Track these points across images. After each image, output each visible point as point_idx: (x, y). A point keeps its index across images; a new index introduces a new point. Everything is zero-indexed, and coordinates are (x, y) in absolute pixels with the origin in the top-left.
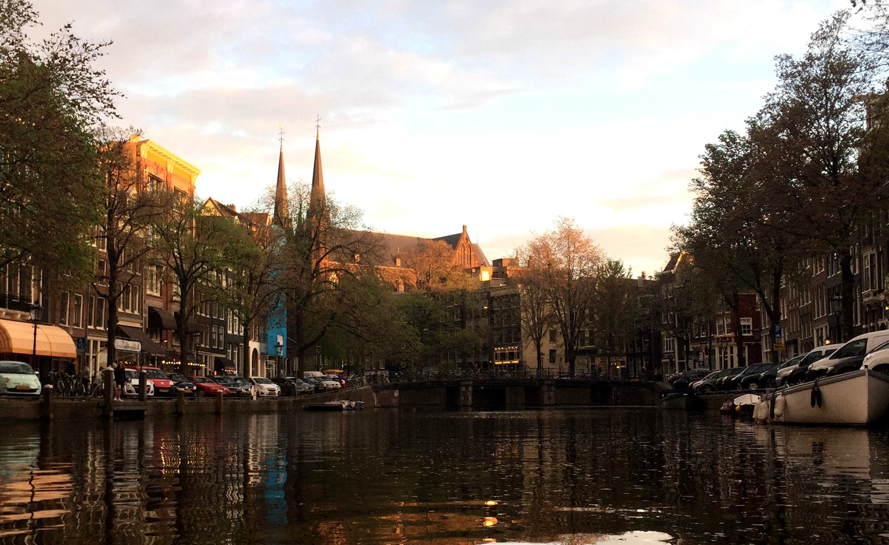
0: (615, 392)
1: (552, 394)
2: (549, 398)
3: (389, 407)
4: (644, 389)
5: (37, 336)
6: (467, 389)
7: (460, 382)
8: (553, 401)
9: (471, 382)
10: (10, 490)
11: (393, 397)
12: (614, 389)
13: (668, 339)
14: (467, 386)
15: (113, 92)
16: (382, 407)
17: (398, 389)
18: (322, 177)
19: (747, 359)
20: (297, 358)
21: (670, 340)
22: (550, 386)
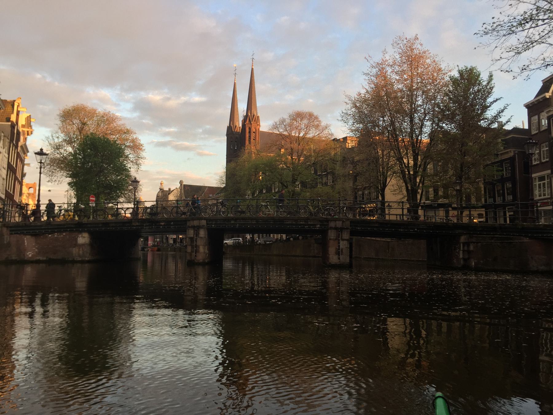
0: (464, 244)
1: (344, 245)
2: (338, 252)
3: (63, 262)
4: (526, 240)
5: (39, 172)
6: (197, 234)
7: (186, 221)
8: (345, 258)
9: (204, 222)
10: (14, 340)
11: (76, 245)
12: (463, 239)
13: (542, 182)
14: (197, 229)
15: (435, 145)
16: (50, 262)
17: (85, 232)
18: (255, 92)
19: (517, 166)
20: (513, 214)
21: (544, 184)
22: (340, 230)
